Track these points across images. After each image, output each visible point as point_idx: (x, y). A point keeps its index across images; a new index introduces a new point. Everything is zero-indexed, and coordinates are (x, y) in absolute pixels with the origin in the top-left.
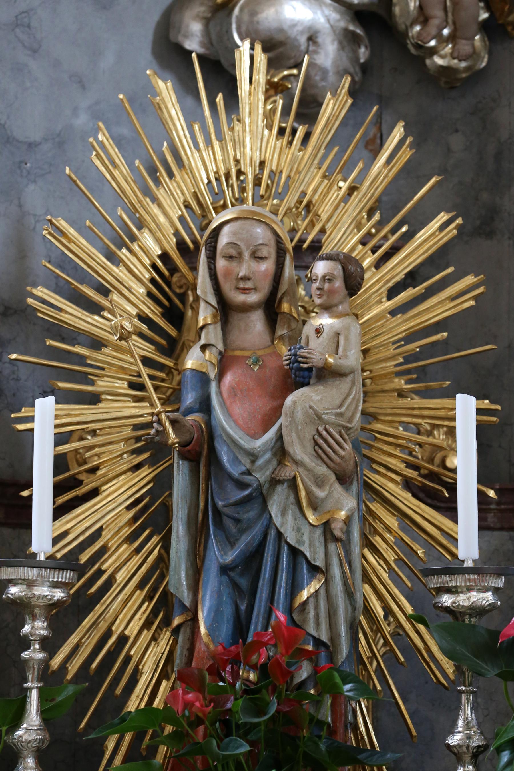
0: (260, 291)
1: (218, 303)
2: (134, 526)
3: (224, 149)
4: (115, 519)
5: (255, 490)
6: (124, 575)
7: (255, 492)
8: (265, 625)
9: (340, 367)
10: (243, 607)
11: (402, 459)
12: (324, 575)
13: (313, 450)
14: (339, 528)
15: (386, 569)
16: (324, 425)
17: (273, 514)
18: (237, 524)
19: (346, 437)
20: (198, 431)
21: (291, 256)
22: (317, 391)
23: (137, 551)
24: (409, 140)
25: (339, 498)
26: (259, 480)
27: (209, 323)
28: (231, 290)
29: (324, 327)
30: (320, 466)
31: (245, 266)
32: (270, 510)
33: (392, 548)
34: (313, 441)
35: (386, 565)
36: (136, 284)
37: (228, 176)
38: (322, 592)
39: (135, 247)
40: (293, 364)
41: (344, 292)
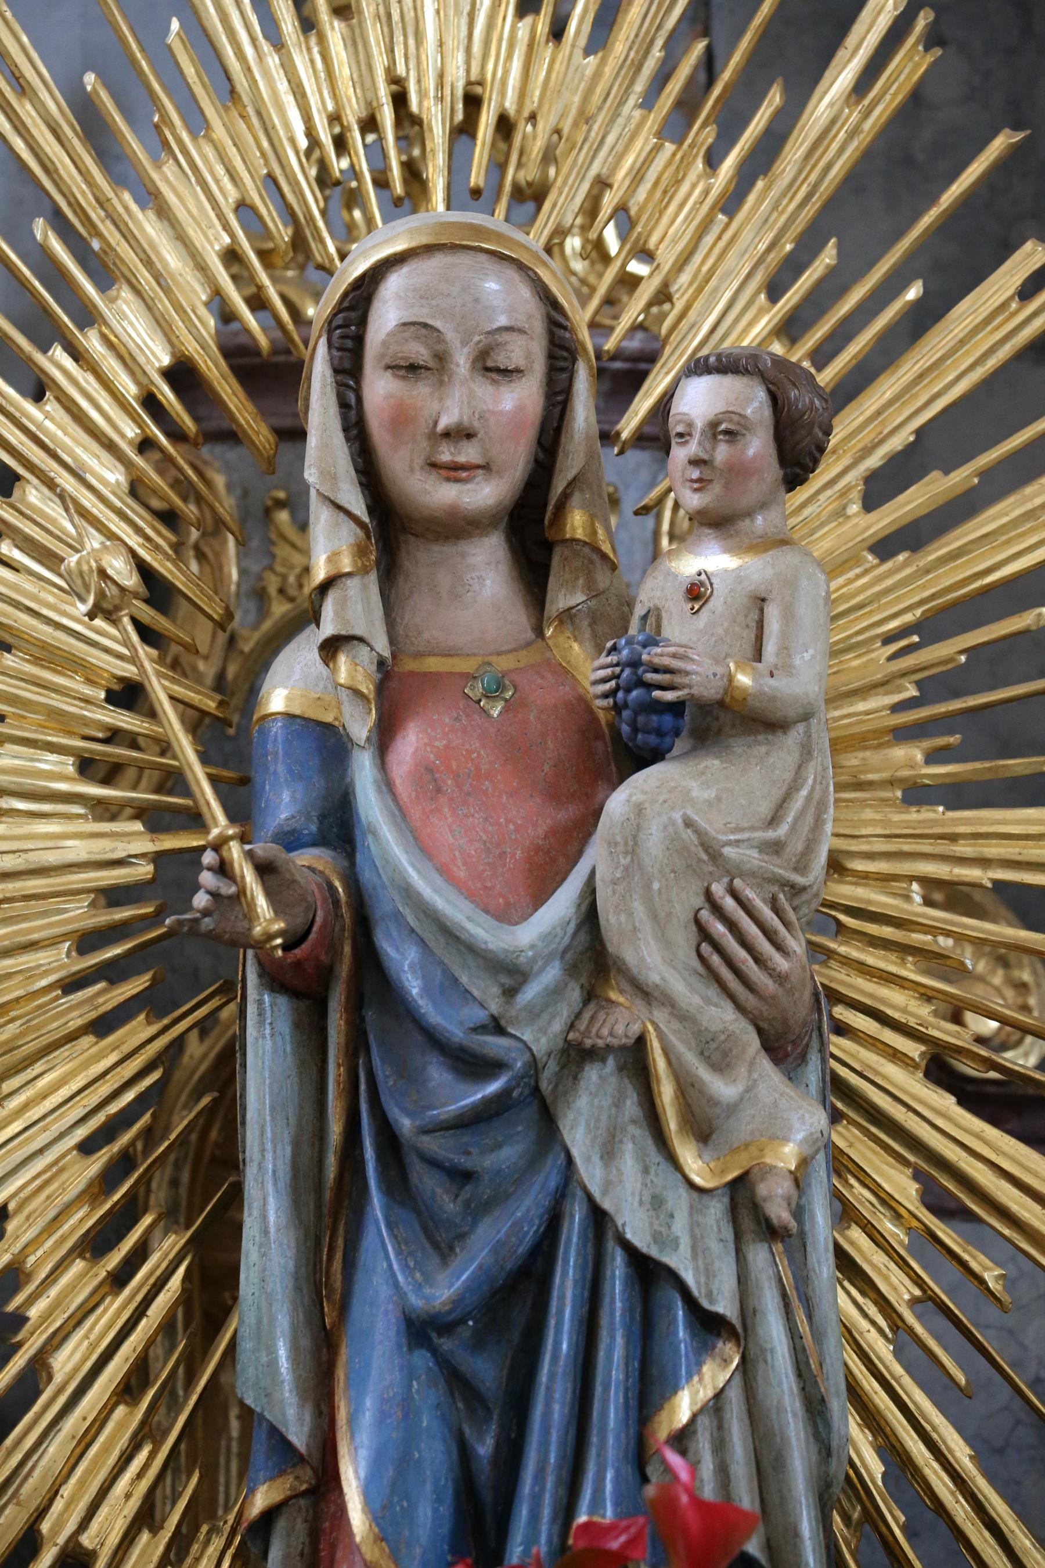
0: (500, 474)
1: (371, 510)
2: (105, 1201)
3: (356, 42)
4: (47, 1183)
5: (519, 1078)
6: (78, 1356)
7: (518, 1085)
8: (565, 1501)
9: (773, 699)
10: (485, 1448)
11: (922, 990)
12: (739, 1345)
13: (694, 954)
14: (782, 1197)
15: (887, 1330)
16: (726, 880)
17: (575, 1152)
18: (461, 1188)
19: (792, 916)
20: (324, 900)
21: (591, 367)
22: (703, 773)
23: (119, 1279)
24: (923, 21)
25: (775, 1104)
26: (530, 1049)
27: (347, 570)
28: (412, 470)
29: (713, 580)
30: (716, 1005)
31: (457, 395)
32: (569, 1143)
33: (903, 1264)
34: (694, 928)
35: (886, 1317)
36: (98, 457)
37: (370, 124)
38: (735, 1396)
39: (92, 342)
40: (628, 691)
41: (773, 471)
